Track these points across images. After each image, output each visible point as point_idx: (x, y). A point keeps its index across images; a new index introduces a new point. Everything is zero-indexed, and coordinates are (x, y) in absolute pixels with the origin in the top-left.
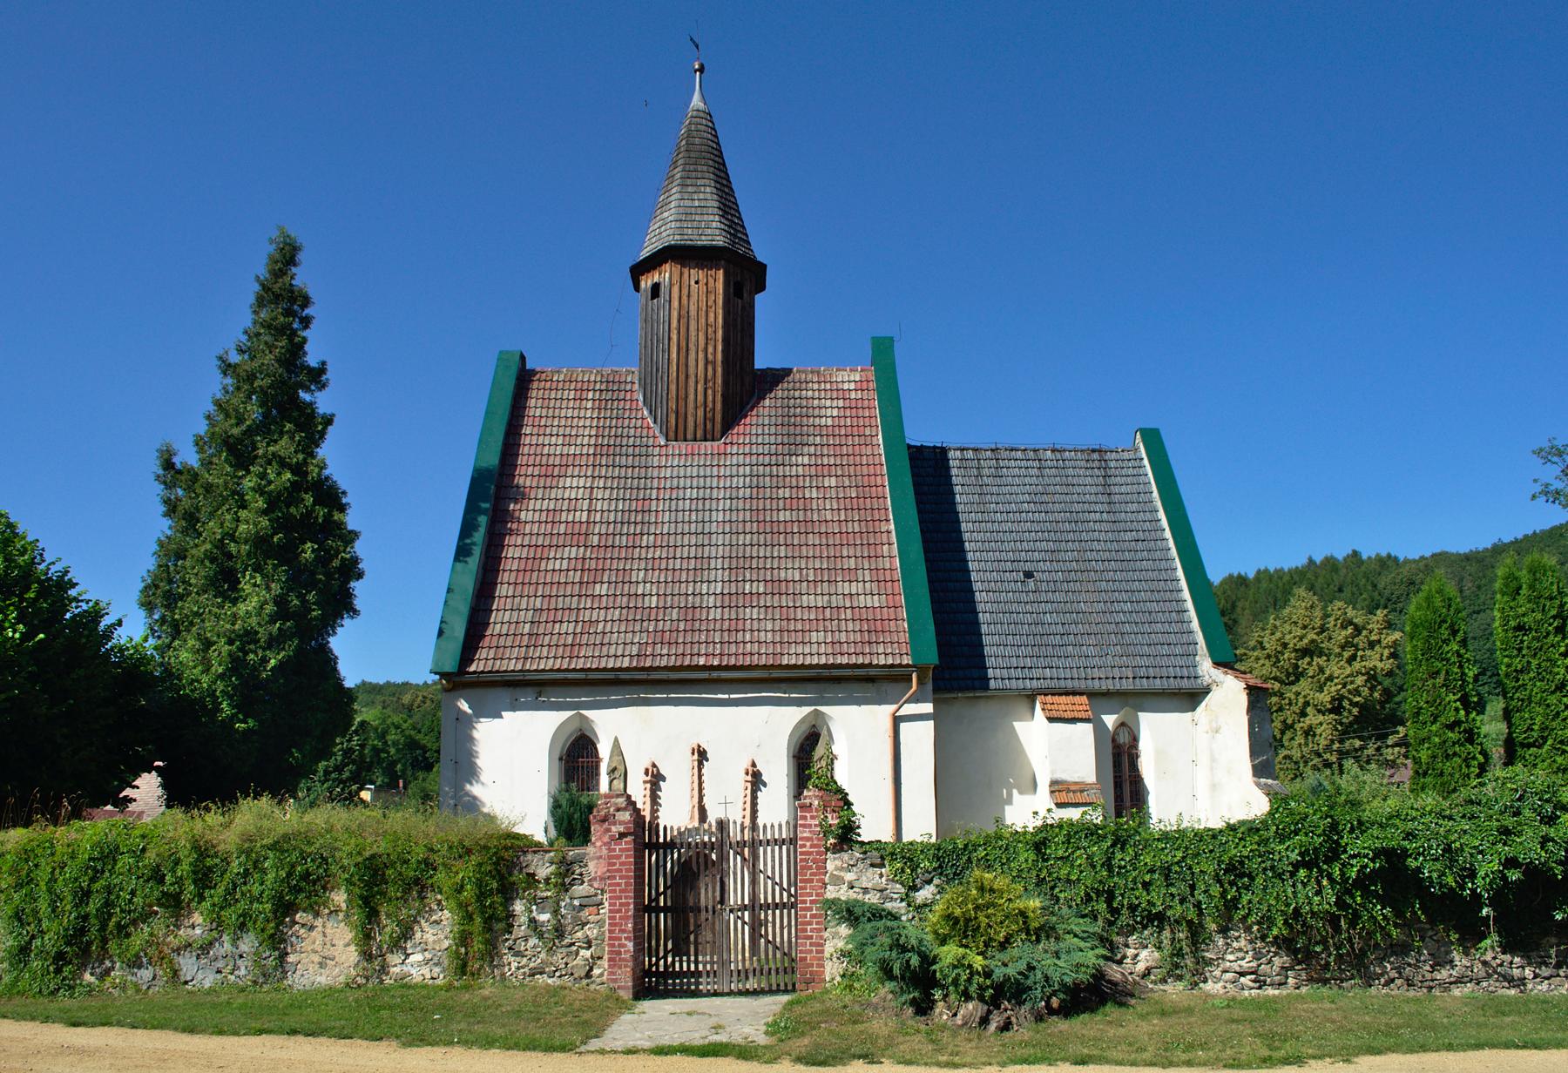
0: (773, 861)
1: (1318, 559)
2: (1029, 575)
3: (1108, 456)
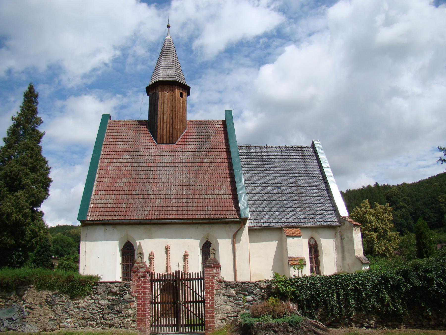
0: (197, 286)
1: (352, 190)
2: (279, 188)
3: (303, 149)
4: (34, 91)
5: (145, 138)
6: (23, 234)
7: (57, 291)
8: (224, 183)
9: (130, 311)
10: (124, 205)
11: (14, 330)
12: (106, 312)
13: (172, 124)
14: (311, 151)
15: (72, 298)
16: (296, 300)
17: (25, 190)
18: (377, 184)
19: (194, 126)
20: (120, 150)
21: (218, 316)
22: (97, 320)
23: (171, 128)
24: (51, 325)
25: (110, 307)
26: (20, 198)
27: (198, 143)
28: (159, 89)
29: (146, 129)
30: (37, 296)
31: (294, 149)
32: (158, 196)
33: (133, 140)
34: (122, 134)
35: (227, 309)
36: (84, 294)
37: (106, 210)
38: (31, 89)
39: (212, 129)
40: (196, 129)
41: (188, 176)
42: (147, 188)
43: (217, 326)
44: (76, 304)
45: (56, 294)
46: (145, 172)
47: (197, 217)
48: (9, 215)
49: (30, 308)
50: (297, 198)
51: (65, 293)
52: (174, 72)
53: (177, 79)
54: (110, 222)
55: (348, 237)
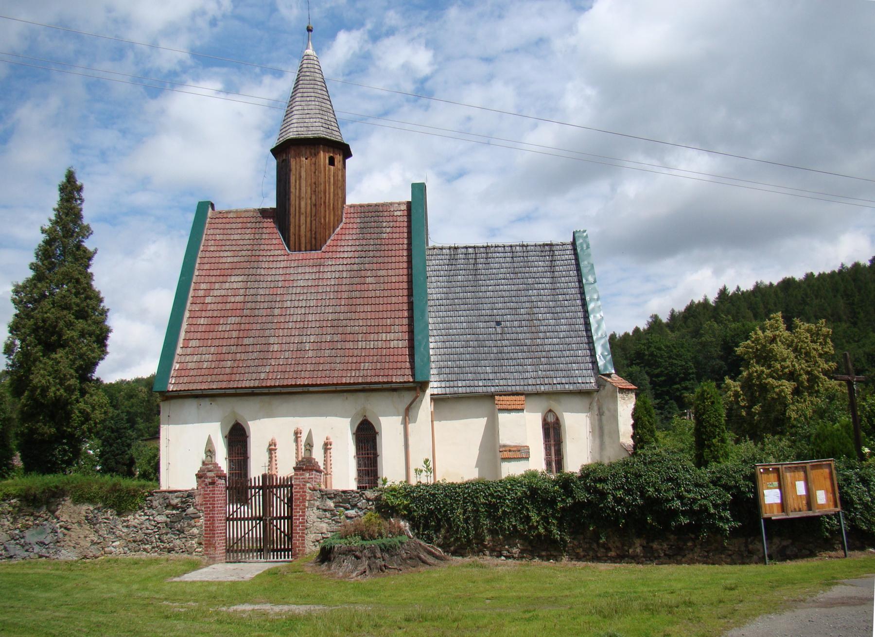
2: (498, 323)
3: (554, 248)
4: (75, 182)
5: (270, 242)
6: (68, 416)
7: (100, 505)
8: (396, 320)
9: (195, 531)
10: (229, 364)
11: (46, 557)
12: (164, 531)
13: (315, 215)
14: (568, 252)
15: (119, 514)
16: (409, 518)
17: (67, 348)
18: (673, 311)
19: (356, 215)
20: (227, 266)
21: (311, 537)
22: (152, 542)
23: (314, 222)
24: (93, 550)
25: (169, 525)
26: (59, 362)
27: (359, 248)
28: (292, 152)
29: (273, 225)
30: (74, 511)
31: (538, 248)
32: (285, 347)
33: (249, 247)
34: (232, 237)
35: (322, 528)
36: (134, 508)
37: (199, 372)
38: (70, 177)
39: (388, 219)
40: (358, 220)
41: (338, 309)
42: (267, 333)
43: (307, 550)
44: (125, 521)
45: (98, 509)
46: (266, 305)
47: (344, 381)
48: (45, 390)
49: (66, 528)
50: (528, 342)
51: (110, 507)
52: (318, 120)
53: (322, 133)
54: (205, 392)
55: (609, 411)
